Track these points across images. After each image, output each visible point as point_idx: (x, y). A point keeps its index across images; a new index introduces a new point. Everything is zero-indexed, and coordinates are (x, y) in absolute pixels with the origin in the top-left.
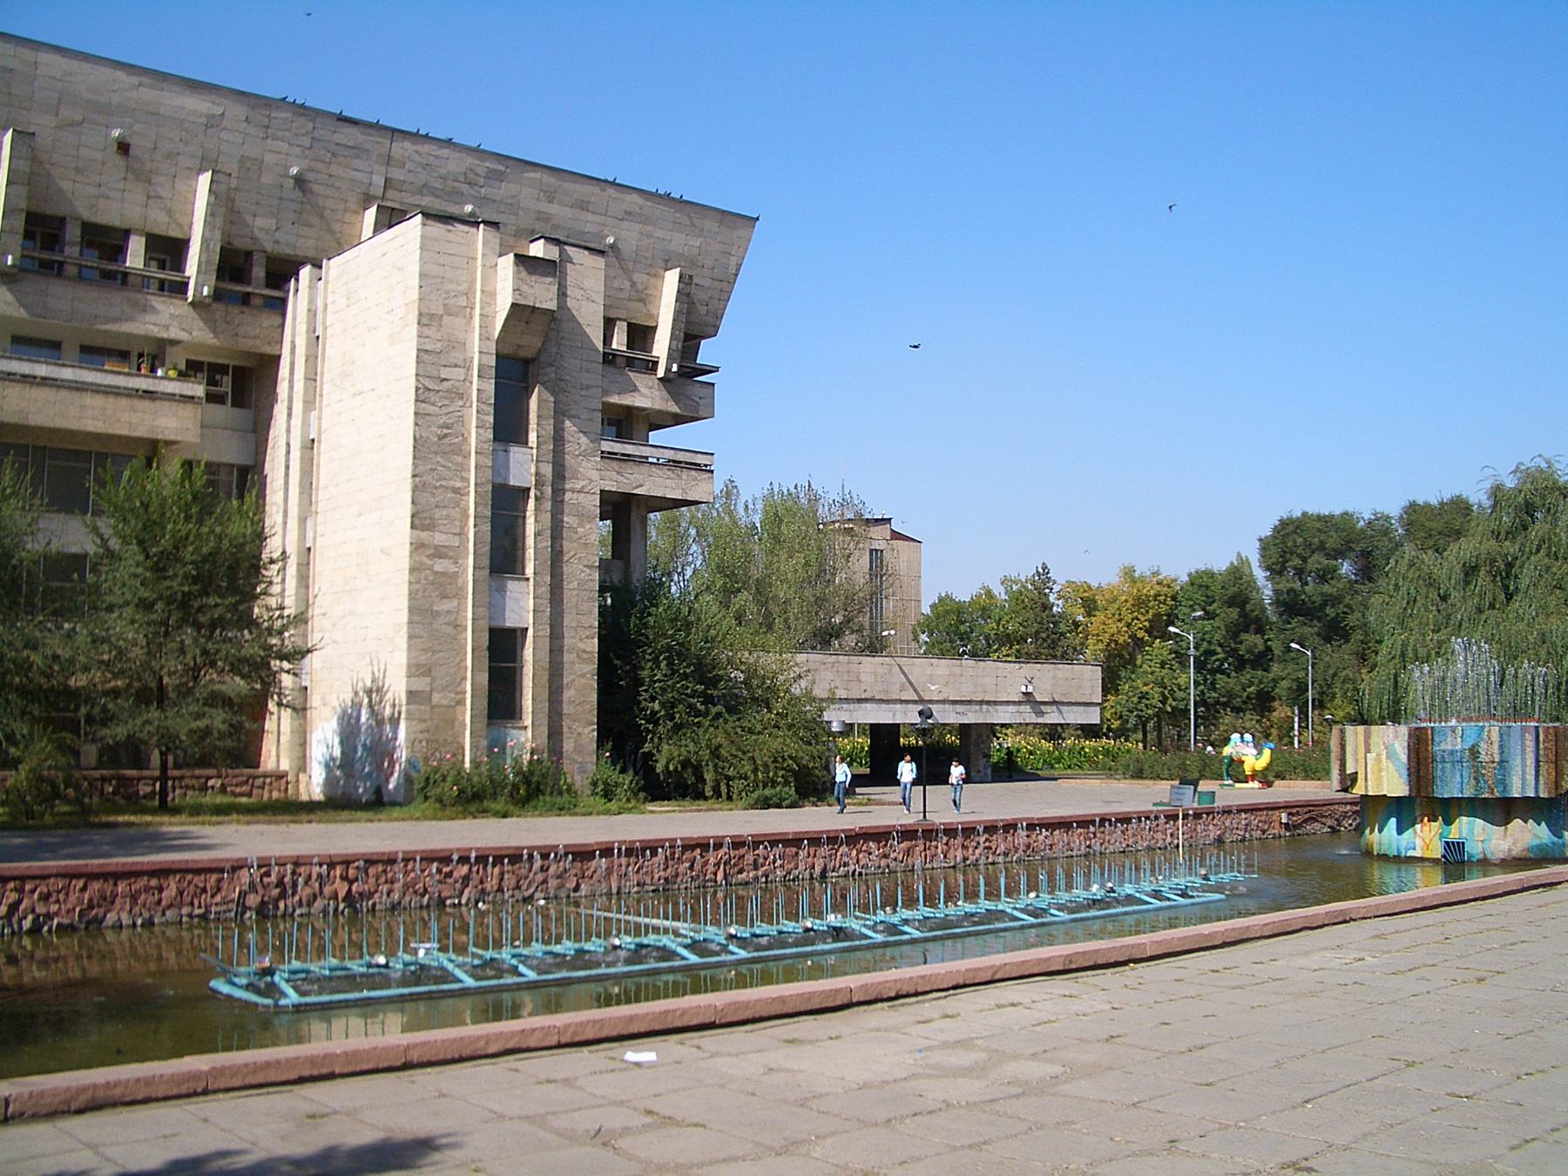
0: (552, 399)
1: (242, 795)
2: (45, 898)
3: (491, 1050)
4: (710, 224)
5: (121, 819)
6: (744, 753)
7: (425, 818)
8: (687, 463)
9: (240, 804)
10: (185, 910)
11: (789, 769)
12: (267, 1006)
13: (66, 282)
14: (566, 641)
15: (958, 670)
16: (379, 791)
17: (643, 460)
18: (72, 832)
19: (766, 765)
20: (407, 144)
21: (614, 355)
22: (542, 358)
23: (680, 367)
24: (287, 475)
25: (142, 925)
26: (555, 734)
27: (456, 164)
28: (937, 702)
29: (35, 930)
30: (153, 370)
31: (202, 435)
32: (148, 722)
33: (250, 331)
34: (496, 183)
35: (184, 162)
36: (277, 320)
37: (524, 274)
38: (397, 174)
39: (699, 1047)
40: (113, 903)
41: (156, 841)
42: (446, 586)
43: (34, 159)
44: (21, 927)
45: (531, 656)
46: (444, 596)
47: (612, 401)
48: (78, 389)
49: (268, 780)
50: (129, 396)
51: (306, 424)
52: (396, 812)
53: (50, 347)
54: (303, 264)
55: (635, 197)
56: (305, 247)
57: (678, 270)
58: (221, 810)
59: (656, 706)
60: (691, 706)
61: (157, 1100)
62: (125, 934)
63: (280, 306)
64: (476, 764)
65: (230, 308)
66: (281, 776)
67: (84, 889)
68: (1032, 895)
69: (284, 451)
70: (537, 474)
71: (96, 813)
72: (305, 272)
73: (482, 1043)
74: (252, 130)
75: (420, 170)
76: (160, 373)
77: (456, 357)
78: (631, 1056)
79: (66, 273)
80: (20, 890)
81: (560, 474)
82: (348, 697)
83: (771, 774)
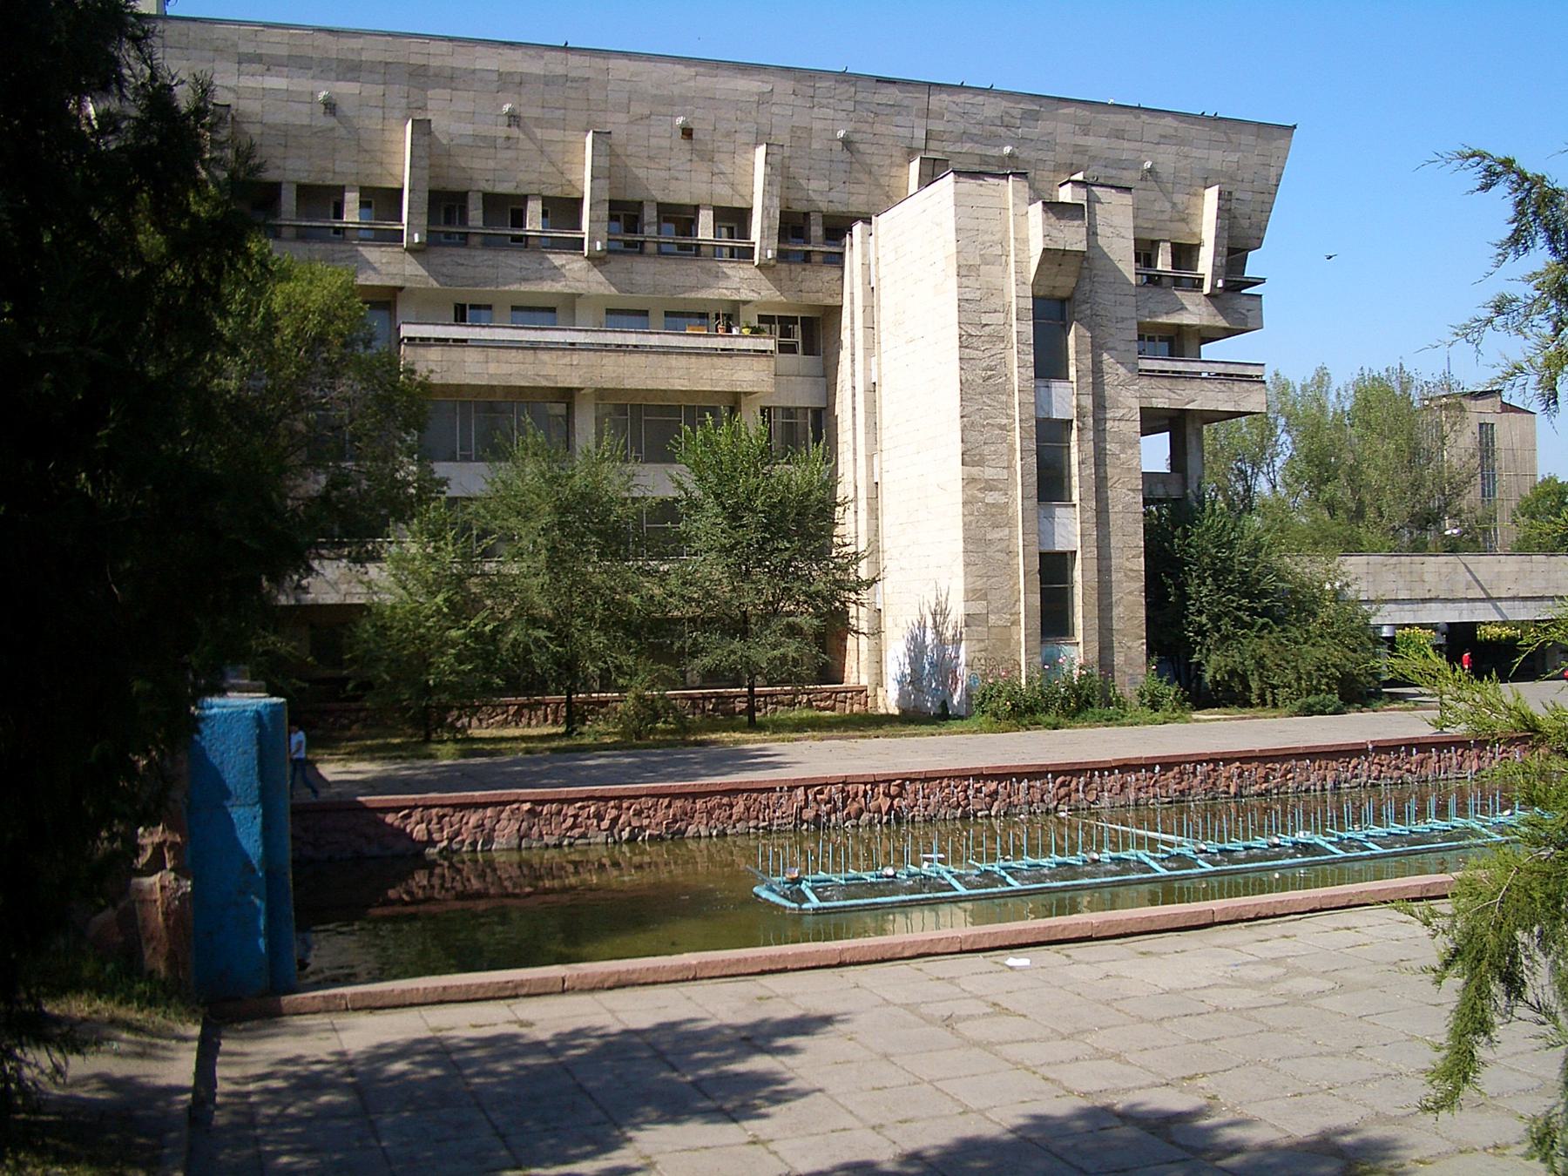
0: (1089, 334)
1: (825, 709)
2: (638, 813)
3: (906, 954)
4: (1247, 139)
5: (713, 736)
6: (1288, 662)
7: (982, 731)
8: (1238, 375)
9: (824, 718)
10: (752, 824)
11: (1331, 677)
12: (794, 909)
13: (647, 259)
14: (1114, 562)
15: (1527, 566)
16: (944, 705)
17: (1195, 376)
18: (670, 750)
19: (1309, 674)
20: (944, 96)
21: (1160, 276)
22: (1077, 296)
23: (1225, 282)
24: (854, 416)
25: (717, 836)
26: (1106, 649)
27: (992, 109)
28: (1506, 599)
29: (632, 840)
30: (729, 330)
31: (777, 384)
32: (733, 652)
33: (812, 286)
34: (1032, 123)
35: (742, 138)
36: (836, 273)
37: (1053, 219)
38: (937, 126)
39: (1068, 956)
40: (693, 818)
41: (740, 759)
42: (996, 516)
43: (612, 154)
44: (621, 838)
45: (1080, 577)
46: (996, 526)
47: (1160, 320)
48: (664, 353)
49: (849, 695)
50: (709, 355)
51: (867, 369)
52: (956, 725)
53: (636, 316)
54: (856, 220)
55: (1169, 120)
56: (857, 204)
57: (1217, 187)
58: (800, 726)
59: (1204, 619)
60: (1238, 619)
61: (662, 983)
62: (703, 843)
63: (837, 260)
64: (1029, 682)
65: (793, 267)
66: (861, 691)
67: (669, 806)
68: (1507, 812)
69: (850, 393)
70: (1078, 406)
71: (700, 730)
72: (858, 228)
73: (900, 948)
74: (799, 102)
75: (958, 119)
76: (735, 331)
77: (995, 302)
78: (1011, 961)
79: (646, 251)
80: (619, 808)
81: (1100, 405)
82: (916, 618)
83: (1314, 682)
